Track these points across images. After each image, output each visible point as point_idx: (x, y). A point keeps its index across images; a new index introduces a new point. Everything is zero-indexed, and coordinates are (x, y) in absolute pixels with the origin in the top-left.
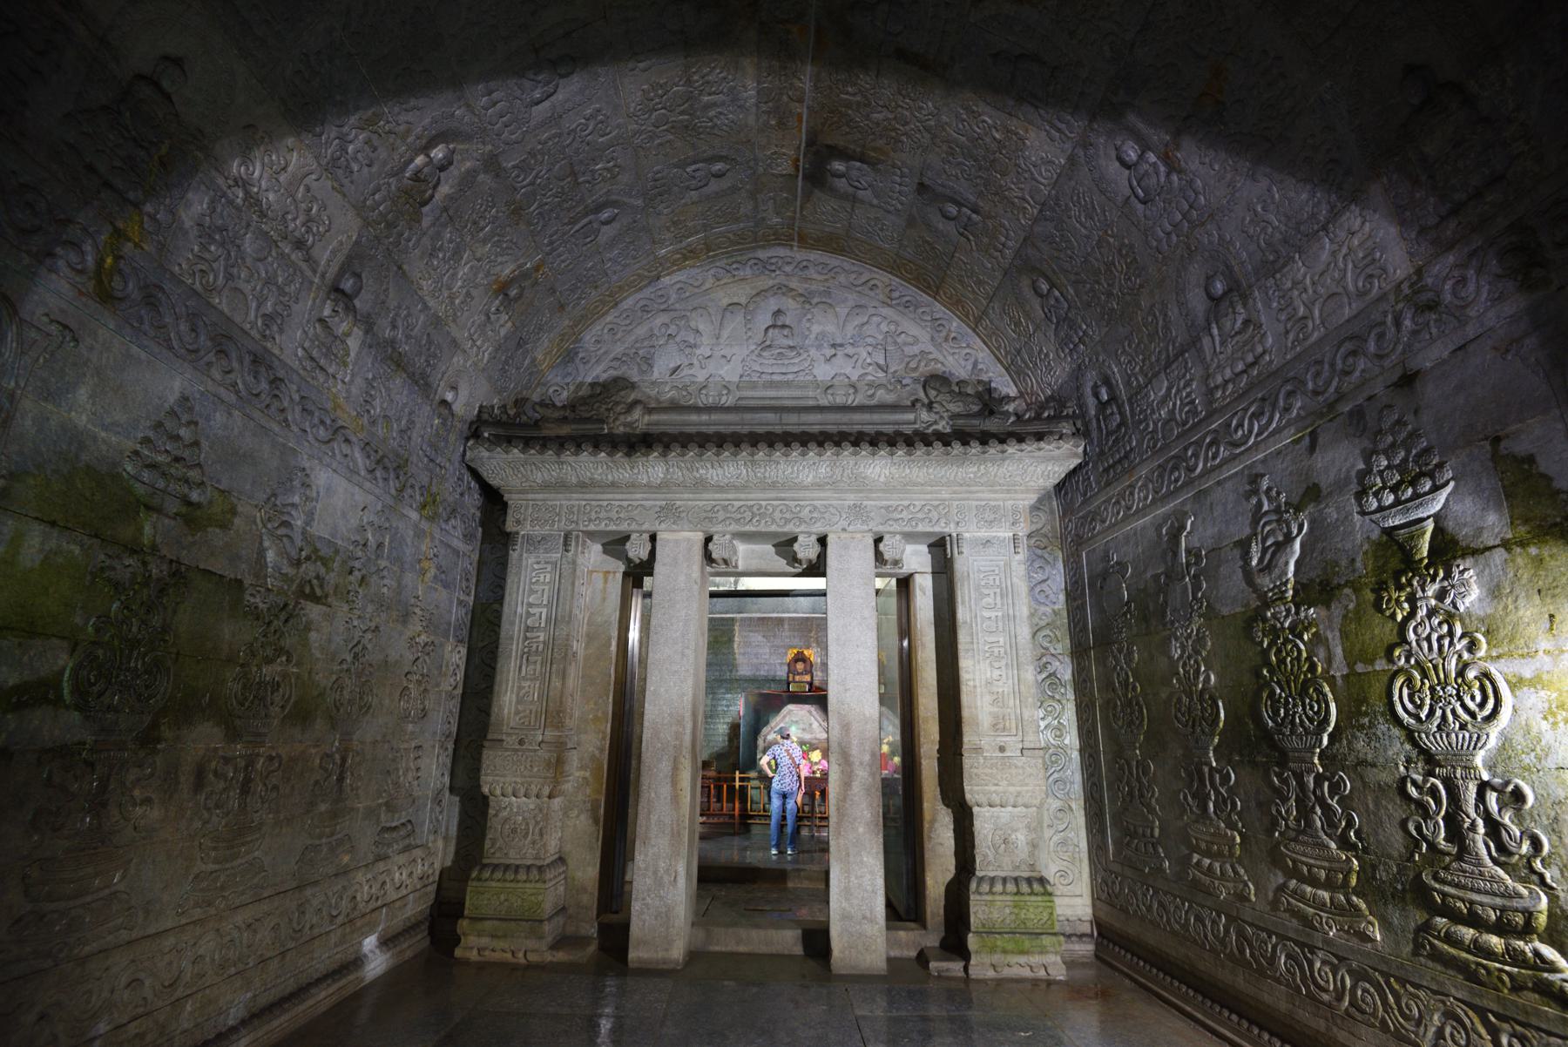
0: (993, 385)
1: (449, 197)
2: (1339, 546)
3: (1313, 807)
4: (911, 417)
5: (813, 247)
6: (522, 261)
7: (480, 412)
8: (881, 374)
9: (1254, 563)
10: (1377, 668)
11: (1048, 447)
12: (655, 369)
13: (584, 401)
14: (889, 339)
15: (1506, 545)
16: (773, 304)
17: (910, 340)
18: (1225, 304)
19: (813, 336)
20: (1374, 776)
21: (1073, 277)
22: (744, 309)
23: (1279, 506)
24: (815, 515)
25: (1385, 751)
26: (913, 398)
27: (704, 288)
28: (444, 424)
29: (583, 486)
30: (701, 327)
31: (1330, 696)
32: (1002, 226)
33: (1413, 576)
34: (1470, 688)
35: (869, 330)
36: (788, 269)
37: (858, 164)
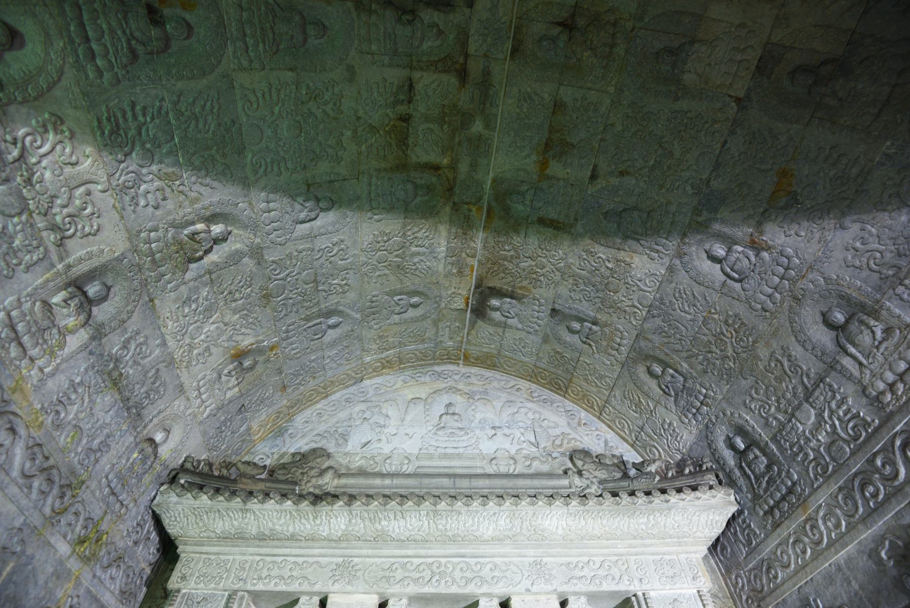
0: (625, 458)
1: (216, 265)
4: (565, 482)
5: (474, 365)
6: (261, 338)
7: (185, 461)
8: (534, 449)
11: (704, 496)
12: (350, 444)
13: (283, 466)
14: (536, 424)
16: (446, 399)
17: (552, 425)
18: (854, 327)
19: (477, 421)
21: (684, 354)
22: (426, 402)
24: (496, 574)
26: (563, 468)
27: (394, 388)
28: (144, 461)
29: (262, 538)
30: (390, 413)
32: (617, 330)
35: (520, 417)
36: (456, 377)
37: (509, 300)
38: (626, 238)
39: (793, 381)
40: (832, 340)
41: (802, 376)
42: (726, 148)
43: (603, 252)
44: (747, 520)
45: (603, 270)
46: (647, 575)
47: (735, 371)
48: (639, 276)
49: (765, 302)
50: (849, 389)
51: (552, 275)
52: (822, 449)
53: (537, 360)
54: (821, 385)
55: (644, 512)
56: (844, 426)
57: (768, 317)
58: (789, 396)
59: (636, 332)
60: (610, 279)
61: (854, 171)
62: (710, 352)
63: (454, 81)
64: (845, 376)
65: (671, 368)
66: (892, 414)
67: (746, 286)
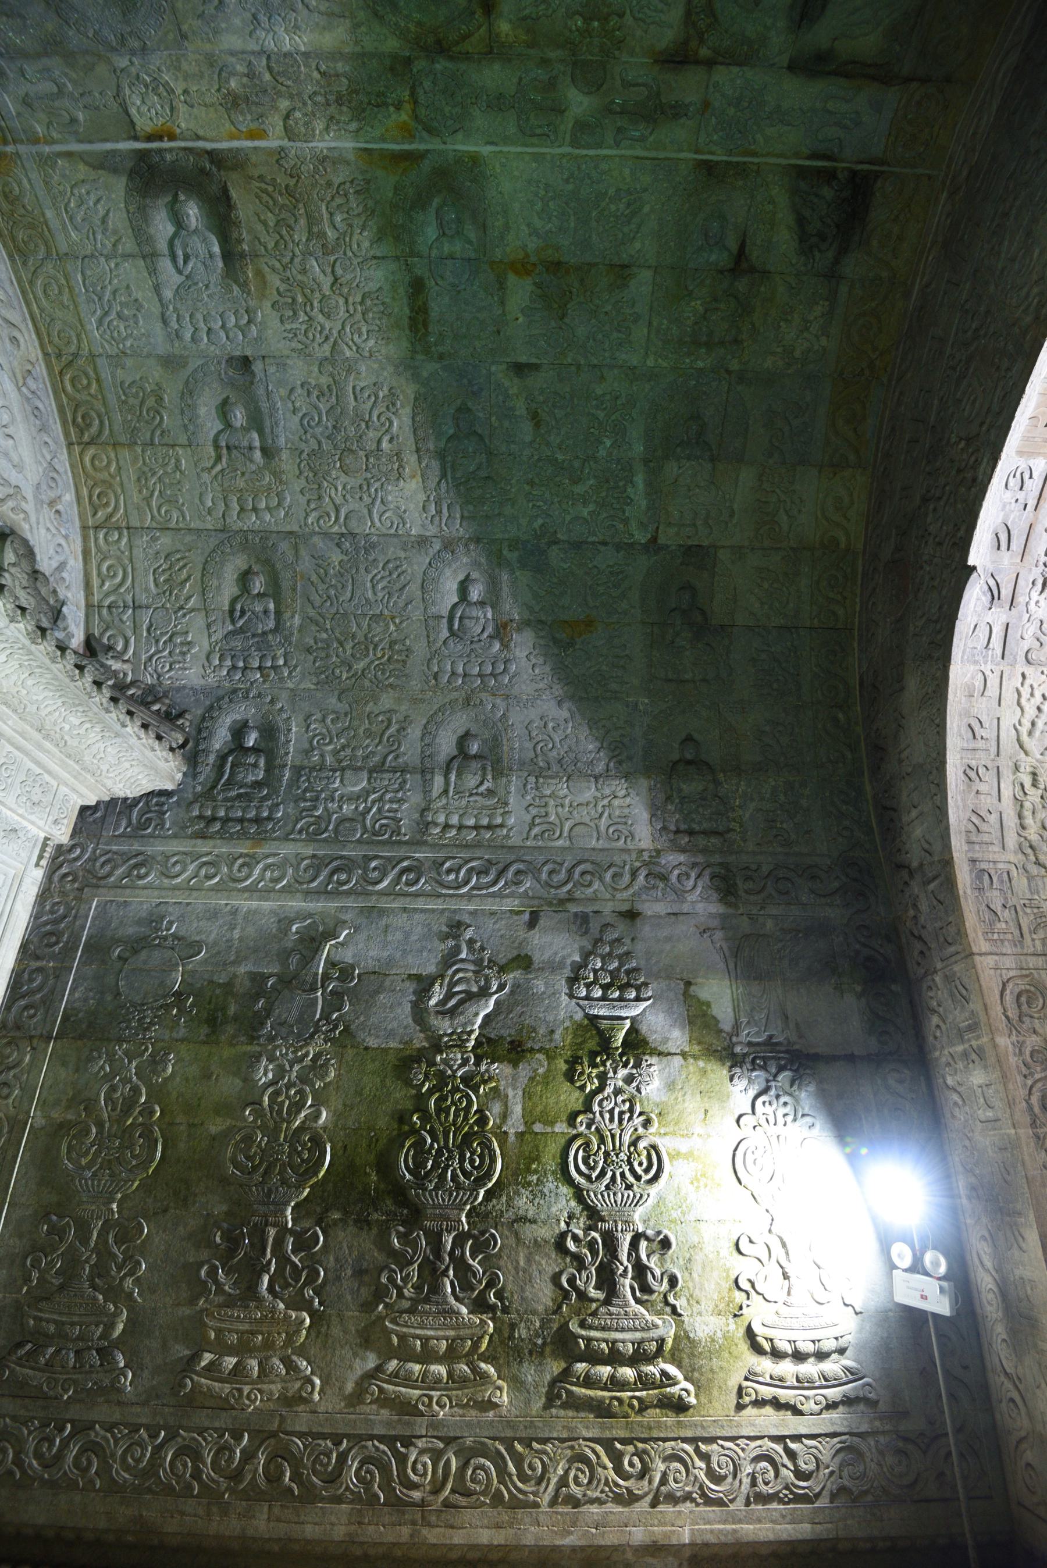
0: (65, 609)
2: (541, 1015)
3: (447, 1269)
9: (433, 1002)
10: (557, 1130)
15: (684, 1055)
18: (475, 765)
20: (529, 1232)
21: (312, 613)
23: (482, 960)
25: (549, 1209)
31: (498, 1152)
33: (608, 1059)
34: (639, 1155)
37: (216, 249)
38: (441, 455)
39: (379, 748)
40: (448, 755)
41: (392, 752)
42: (600, 547)
43: (401, 423)
44: (166, 807)
45: (371, 434)
46: (9, 781)
47: (339, 684)
48: (390, 498)
49: (445, 672)
50: (415, 798)
51: (319, 339)
52: (335, 816)
53: (108, 356)
54: (399, 774)
55: (89, 714)
56: (377, 817)
57: (431, 684)
58: (360, 753)
59: (296, 528)
60: (362, 453)
61: (614, 686)
62: (341, 644)
63: (667, 37)
64: (424, 787)
65: (277, 604)
66: (425, 843)
67: (451, 642)
